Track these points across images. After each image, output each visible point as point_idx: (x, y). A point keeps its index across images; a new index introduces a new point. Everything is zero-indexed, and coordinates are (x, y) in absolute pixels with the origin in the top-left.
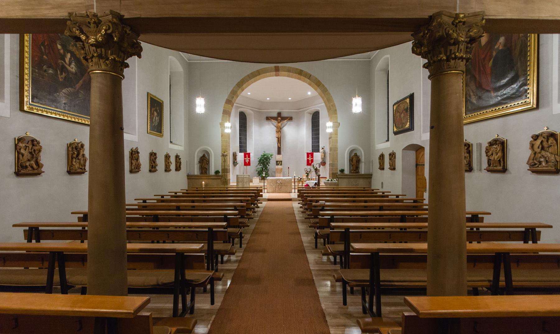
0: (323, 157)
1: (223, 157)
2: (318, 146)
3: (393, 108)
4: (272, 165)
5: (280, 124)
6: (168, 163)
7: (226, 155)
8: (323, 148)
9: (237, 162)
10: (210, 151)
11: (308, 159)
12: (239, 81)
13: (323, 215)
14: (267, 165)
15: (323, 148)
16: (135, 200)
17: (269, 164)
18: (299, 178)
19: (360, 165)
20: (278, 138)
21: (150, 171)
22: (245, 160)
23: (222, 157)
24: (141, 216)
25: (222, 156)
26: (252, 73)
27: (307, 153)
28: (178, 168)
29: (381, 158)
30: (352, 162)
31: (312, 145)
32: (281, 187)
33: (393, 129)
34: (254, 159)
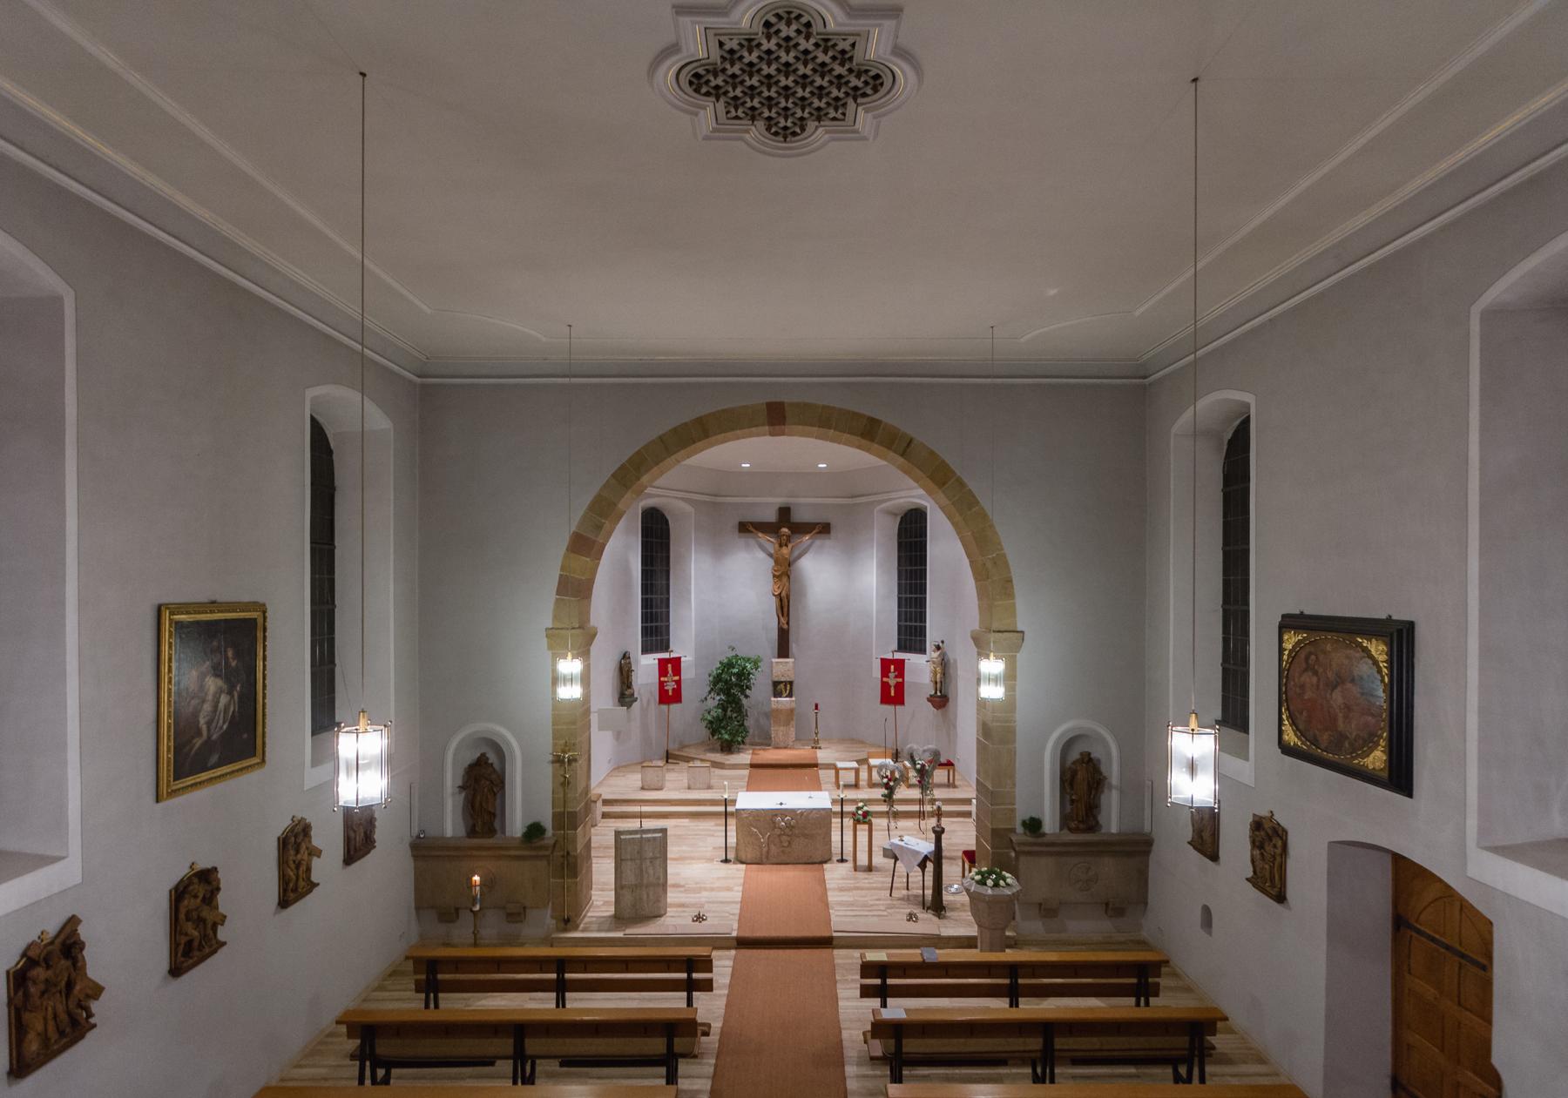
0: (938, 680)
1: (558, 765)
2: (922, 632)
3: (1281, 650)
4: (758, 695)
5: (785, 551)
7: (572, 761)
8: (938, 648)
9: (633, 694)
10: (508, 744)
11: (885, 679)
12: (625, 459)
14: (742, 697)
15: (938, 648)
17: (748, 692)
18: (860, 812)
19: (1104, 798)
20: (779, 597)
22: (661, 684)
23: (553, 767)
25: (553, 762)
26: (675, 430)
27: (882, 660)
30: (1071, 784)
31: (899, 627)
32: (789, 843)
33: (1280, 732)
34: (694, 676)
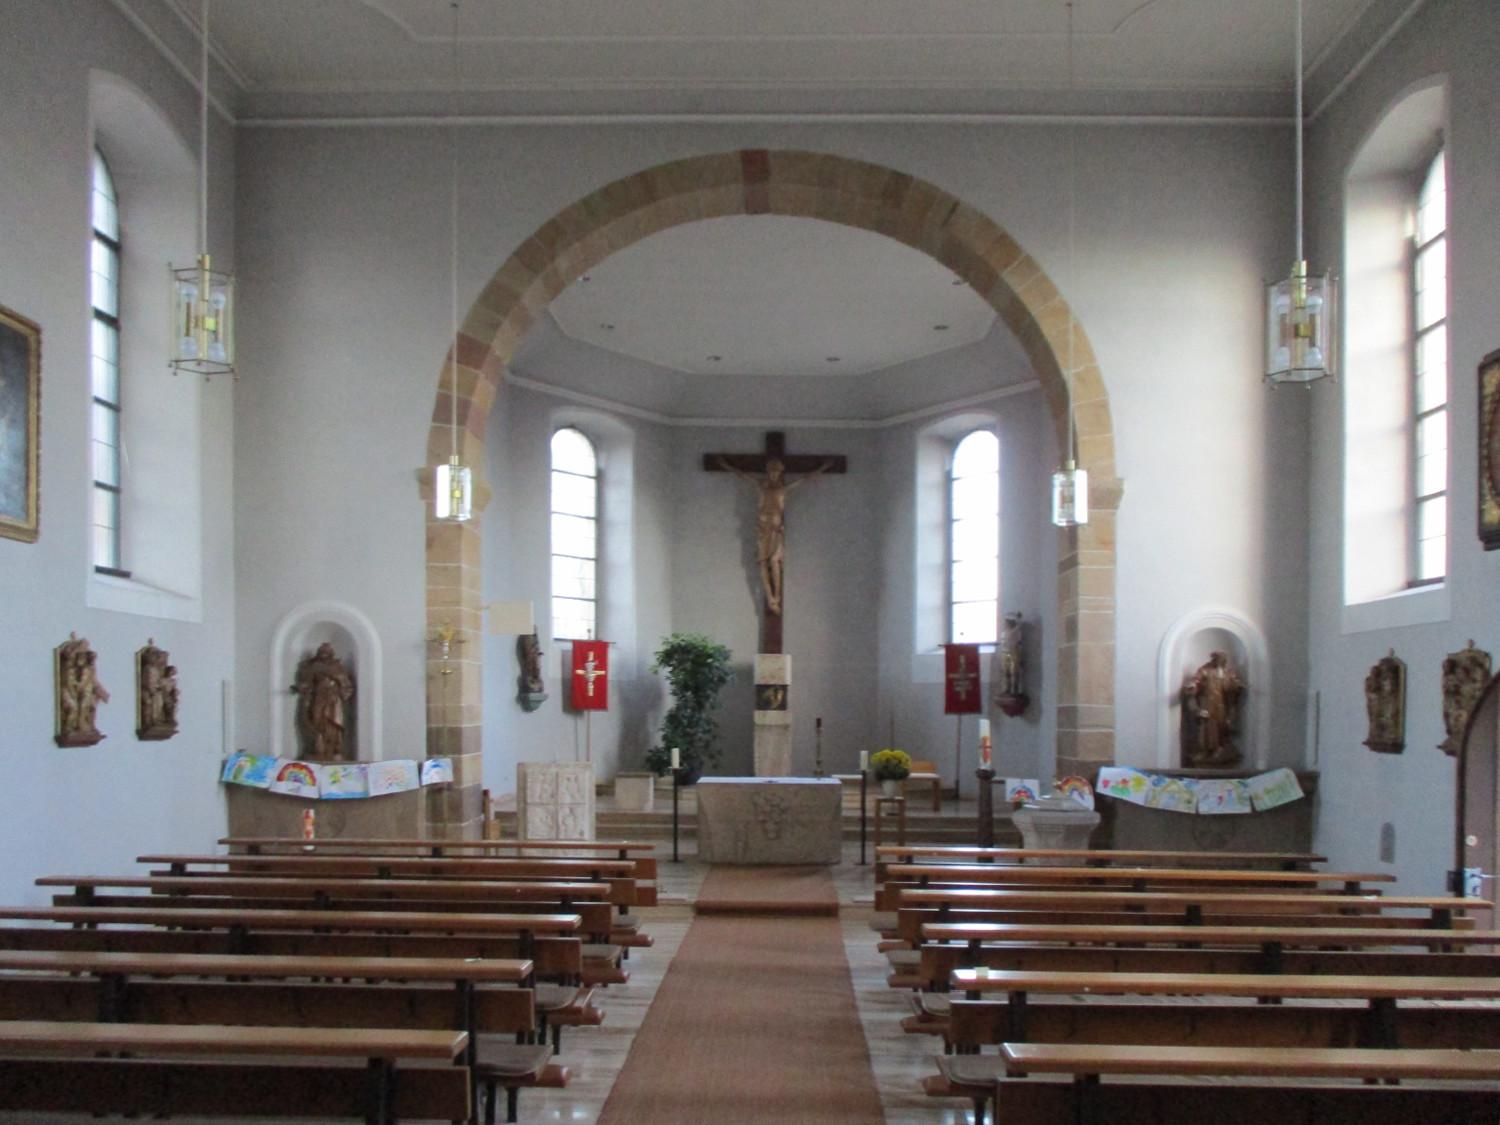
0: (1012, 671)
3: (1481, 386)
6: (80, 697)
13: (945, 937)
16: (141, 860)
21: (62, 740)
24: (164, 929)
28: (156, 723)
29: (1387, 685)
